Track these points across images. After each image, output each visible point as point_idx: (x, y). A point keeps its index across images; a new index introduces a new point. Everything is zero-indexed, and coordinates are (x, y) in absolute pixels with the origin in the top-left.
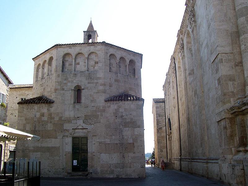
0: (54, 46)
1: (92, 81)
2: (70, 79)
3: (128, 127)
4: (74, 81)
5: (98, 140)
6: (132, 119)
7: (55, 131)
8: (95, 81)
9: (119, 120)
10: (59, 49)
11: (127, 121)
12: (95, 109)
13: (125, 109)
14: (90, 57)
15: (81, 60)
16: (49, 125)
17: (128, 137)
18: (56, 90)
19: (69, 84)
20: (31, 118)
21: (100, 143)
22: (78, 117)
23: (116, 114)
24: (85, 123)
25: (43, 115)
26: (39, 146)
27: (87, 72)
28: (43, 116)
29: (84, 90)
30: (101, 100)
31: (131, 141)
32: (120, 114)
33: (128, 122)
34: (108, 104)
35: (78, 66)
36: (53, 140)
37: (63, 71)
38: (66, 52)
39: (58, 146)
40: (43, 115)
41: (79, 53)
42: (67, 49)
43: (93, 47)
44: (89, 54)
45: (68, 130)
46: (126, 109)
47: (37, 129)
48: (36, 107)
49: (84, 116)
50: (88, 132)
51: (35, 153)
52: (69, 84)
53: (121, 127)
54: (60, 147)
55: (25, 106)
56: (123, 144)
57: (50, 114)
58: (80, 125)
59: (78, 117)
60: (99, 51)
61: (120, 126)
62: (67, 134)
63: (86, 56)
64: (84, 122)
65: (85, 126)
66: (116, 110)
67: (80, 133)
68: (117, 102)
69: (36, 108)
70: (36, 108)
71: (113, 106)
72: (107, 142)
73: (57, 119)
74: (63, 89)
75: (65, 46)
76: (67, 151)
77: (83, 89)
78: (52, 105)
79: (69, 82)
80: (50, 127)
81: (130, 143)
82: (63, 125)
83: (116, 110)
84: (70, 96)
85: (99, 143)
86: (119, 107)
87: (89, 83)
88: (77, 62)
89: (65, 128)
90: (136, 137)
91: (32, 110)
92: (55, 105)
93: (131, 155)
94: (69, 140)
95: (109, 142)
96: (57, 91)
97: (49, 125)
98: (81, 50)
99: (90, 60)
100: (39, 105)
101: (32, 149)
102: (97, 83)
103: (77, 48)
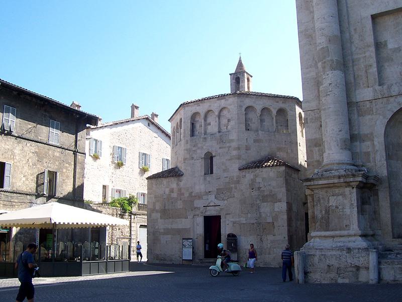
0: (180, 106)
1: (224, 145)
2: (199, 145)
3: (267, 202)
4: (204, 147)
5: (232, 220)
6: (271, 191)
7: (185, 209)
8: (228, 145)
9: (255, 193)
10: (187, 108)
11: (266, 194)
12: (227, 180)
13: (263, 179)
14: (221, 114)
15: (212, 120)
16: (179, 202)
17: (267, 215)
18: (185, 159)
19: (199, 151)
20: (161, 195)
21: (234, 223)
22: (209, 192)
23: (252, 186)
24: (217, 199)
25: (172, 191)
26: (170, 228)
27: (218, 135)
28: (173, 192)
29: (216, 157)
30: (235, 166)
31: (270, 220)
32: (257, 186)
33: (267, 195)
34: (243, 173)
35: (209, 127)
36: (184, 220)
37: (193, 134)
38: (194, 111)
39: (189, 227)
40: (172, 191)
41: (209, 111)
42: (195, 107)
43: (224, 100)
44: (221, 111)
45: (198, 208)
46: (264, 178)
47: (166, 208)
48: (165, 181)
49: (216, 190)
50: (221, 209)
51: (166, 236)
52: (199, 151)
53: (258, 202)
54: (191, 229)
55: (154, 181)
56: (260, 224)
57: (180, 190)
58: (212, 201)
59: (209, 192)
60: (231, 105)
61: (256, 201)
62: (197, 213)
63: (217, 113)
64: (216, 198)
65: (218, 202)
66: (252, 180)
67: (212, 212)
68: (253, 170)
69: (165, 183)
70: (165, 183)
71: (249, 175)
72: (242, 222)
73: (187, 195)
74: (193, 158)
75: (192, 104)
76: (198, 233)
77: (214, 156)
78: (181, 178)
79: (199, 148)
80: (180, 205)
81: (269, 223)
82: (193, 202)
83: (252, 180)
84: (200, 166)
85: (233, 223)
86: (256, 176)
87: (220, 148)
88: (208, 122)
89: (195, 206)
90: (276, 215)
91: (160, 186)
92: (184, 178)
93: (270, 237)
94: (200, 221)
95: (244, 222)
96: (186, 161)
97: (179, 202)
98: (210, 106)
99: (223, 118)
100: (167, 180)
101: (162, 231)
102: (230, 147)
103: (205, 104)
